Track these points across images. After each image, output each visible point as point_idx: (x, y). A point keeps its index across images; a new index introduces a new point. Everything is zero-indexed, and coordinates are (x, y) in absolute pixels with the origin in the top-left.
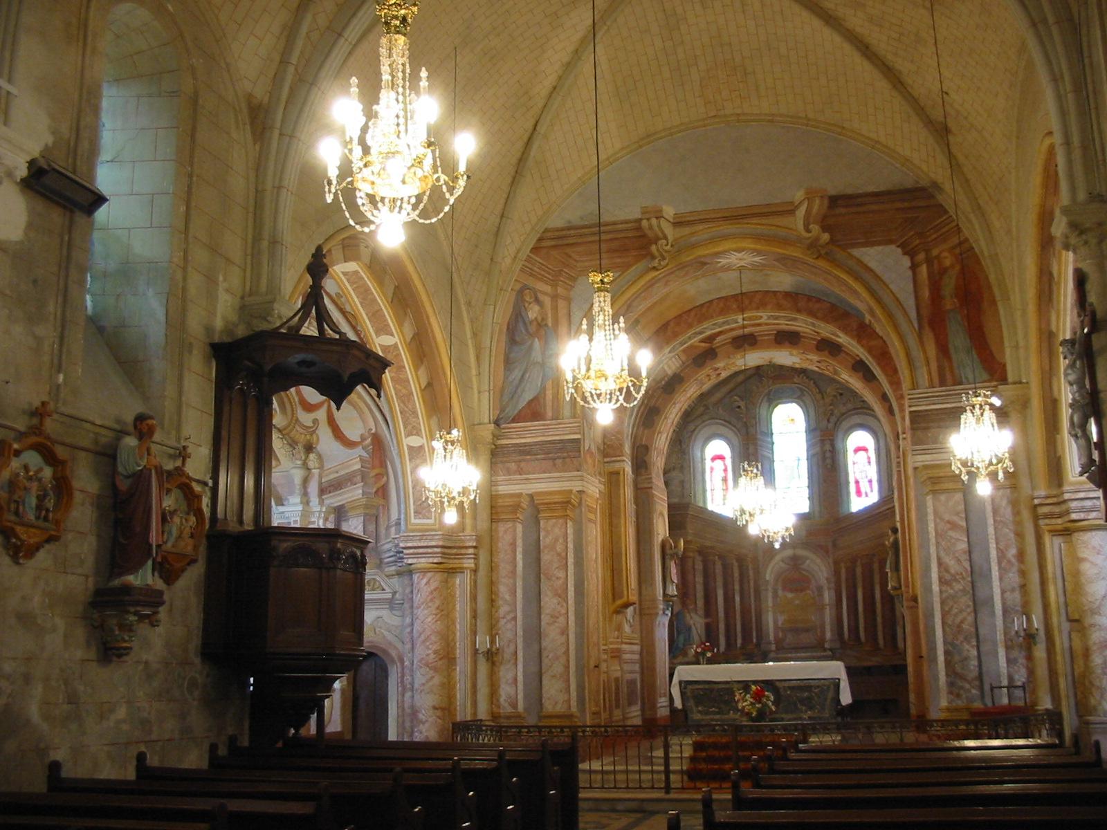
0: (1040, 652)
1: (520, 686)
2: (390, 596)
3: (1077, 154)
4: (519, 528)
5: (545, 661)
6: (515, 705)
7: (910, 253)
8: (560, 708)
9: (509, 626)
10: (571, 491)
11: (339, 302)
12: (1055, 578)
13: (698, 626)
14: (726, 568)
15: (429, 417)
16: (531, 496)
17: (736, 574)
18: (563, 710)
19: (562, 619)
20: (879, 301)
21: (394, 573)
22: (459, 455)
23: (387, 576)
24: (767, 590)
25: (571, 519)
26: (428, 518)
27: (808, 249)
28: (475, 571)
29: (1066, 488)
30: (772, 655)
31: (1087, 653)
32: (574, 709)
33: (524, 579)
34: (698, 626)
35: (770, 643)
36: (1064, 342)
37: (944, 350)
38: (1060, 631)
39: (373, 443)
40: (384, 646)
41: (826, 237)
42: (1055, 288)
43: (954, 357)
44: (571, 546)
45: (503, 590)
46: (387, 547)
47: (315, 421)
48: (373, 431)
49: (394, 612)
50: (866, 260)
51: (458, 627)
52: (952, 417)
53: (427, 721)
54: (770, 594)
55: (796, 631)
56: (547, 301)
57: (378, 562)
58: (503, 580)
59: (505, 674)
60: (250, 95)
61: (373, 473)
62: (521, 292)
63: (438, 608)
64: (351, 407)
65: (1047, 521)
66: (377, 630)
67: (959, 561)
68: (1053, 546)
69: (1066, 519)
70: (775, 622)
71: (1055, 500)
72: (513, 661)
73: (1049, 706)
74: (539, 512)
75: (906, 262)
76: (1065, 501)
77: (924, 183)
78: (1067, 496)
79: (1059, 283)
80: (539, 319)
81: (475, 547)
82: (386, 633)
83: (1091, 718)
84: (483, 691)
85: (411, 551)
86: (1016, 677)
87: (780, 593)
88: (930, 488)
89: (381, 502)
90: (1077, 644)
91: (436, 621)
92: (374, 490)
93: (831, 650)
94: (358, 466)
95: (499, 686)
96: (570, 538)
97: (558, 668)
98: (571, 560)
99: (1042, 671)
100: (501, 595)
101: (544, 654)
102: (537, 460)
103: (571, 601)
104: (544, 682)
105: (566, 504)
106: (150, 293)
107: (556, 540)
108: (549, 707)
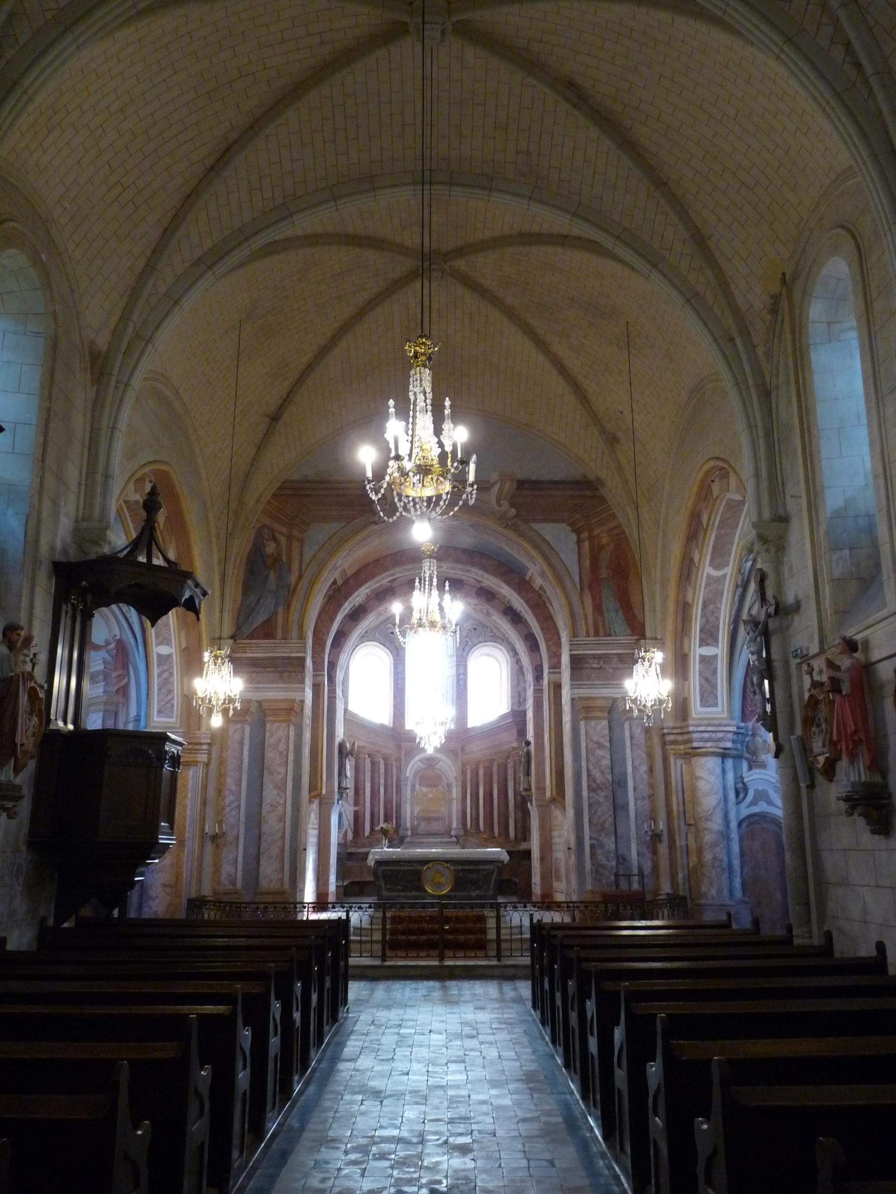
0: (663, 849)
1: (240, 867)
3: (764, 484)
4: (247, 729)
5: (264, 845)
6: (234, 884)
7: (577, 531)
8: (274, 886)
9: (233, 813)
12: (677, 788)
13: (348, 813)
14: (373, 764)
15: (179, 631)
16: (260, 703)
17: (382, 771)
19: (280, 808)
20: (551, 565)
22: (227, 668)
24: (406, 784)
25: (294, 724)
27: (499, 519)
28: (207, 765)
29: (690, 722)
30: (408, 839)
31: (700, 851)
32: (286, 886)
34: (348, 813)
35: (406, 829)
36: (745, 622)
37: (598, 608)
38: (680, 833)
39: (116, 648)
41: (513, 511)
42: (694, 570)
43: (606, 615)
44: (291, 746)
45: (230, 782)
48: (118, 637)
50: (543, 533)
51: (188, 813)
52: (628, 662)
53: (157, 897)
54: (409, 788)
55: (428, 820)
56: (283, 540)
58: (230, 773)
59: (227, 854)
60: (92, 343)
61: (114, 675)
62: (259, 532)
65: (673, 747)
67: (602, 773)
68: (676, 765)
69: (689, 745)
70: (412, 812)
71: (679, 731)
73: (669, 891)
74: (265, 716)
75: (574, 537)
76: (689, 733)
77: (592, 477)
78: (691, 729)
79: (698, 568)
80: (275, 554)
81: (209, 744)
83: (703, 901)
84: (208, 868)
86: (645, 867)
87: (417, 787)
88: (583, 715)
89: (121, 700)
90: (692, 843)
92: (116, 689)
93: (456, 836)
94: (101, 667)
96: (292, 740)
97: (275, 851)
98: (291, 757)
99: (664, 864)
101: (263, 838)
102: (268, 672)
103: (289, 794)
104: (262, 862)
106: (10, 512)
107: (280, 740)
108: (264, 884)
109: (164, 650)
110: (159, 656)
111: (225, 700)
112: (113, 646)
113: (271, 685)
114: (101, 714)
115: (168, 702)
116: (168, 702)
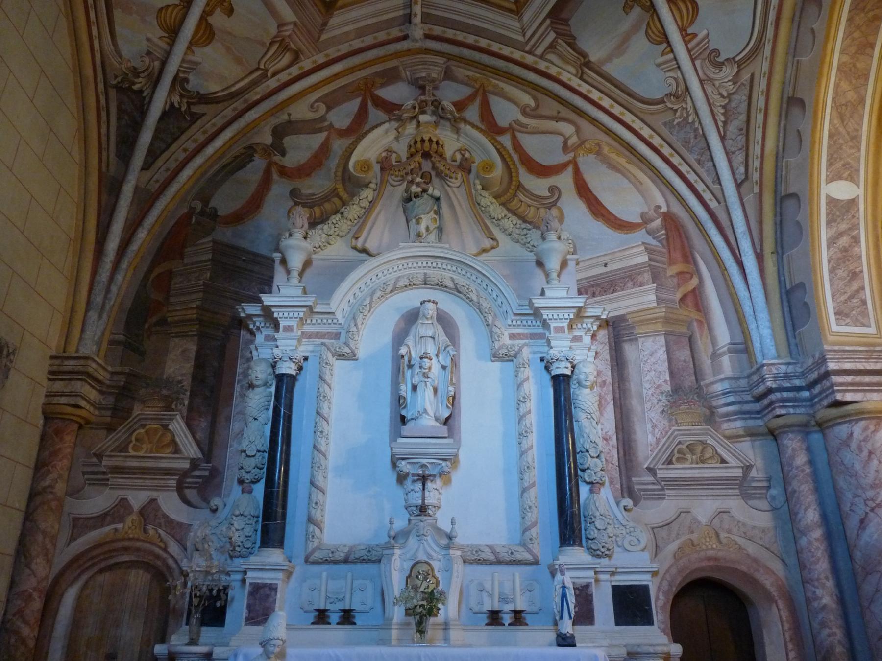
2: (739, 473)
11: (81, 355)
21: (741, 432)
23: (728, 438)
26: (864, 325)
40: (743, 568)
46: (719, 387)
47: (553, 189)
49: (750, 503)
57: (708, 412)
61: (672, 270)
64: (619, 175)
66: (723, 535)
82: (741, 541)
85: (849, 379)
89: (694, 315)
92: (678, 296)
109: (842, 190)
110: (832, 202)
112: (658, 223)
114: (662, 340)
115: (852, 297)
116: (852, 297)
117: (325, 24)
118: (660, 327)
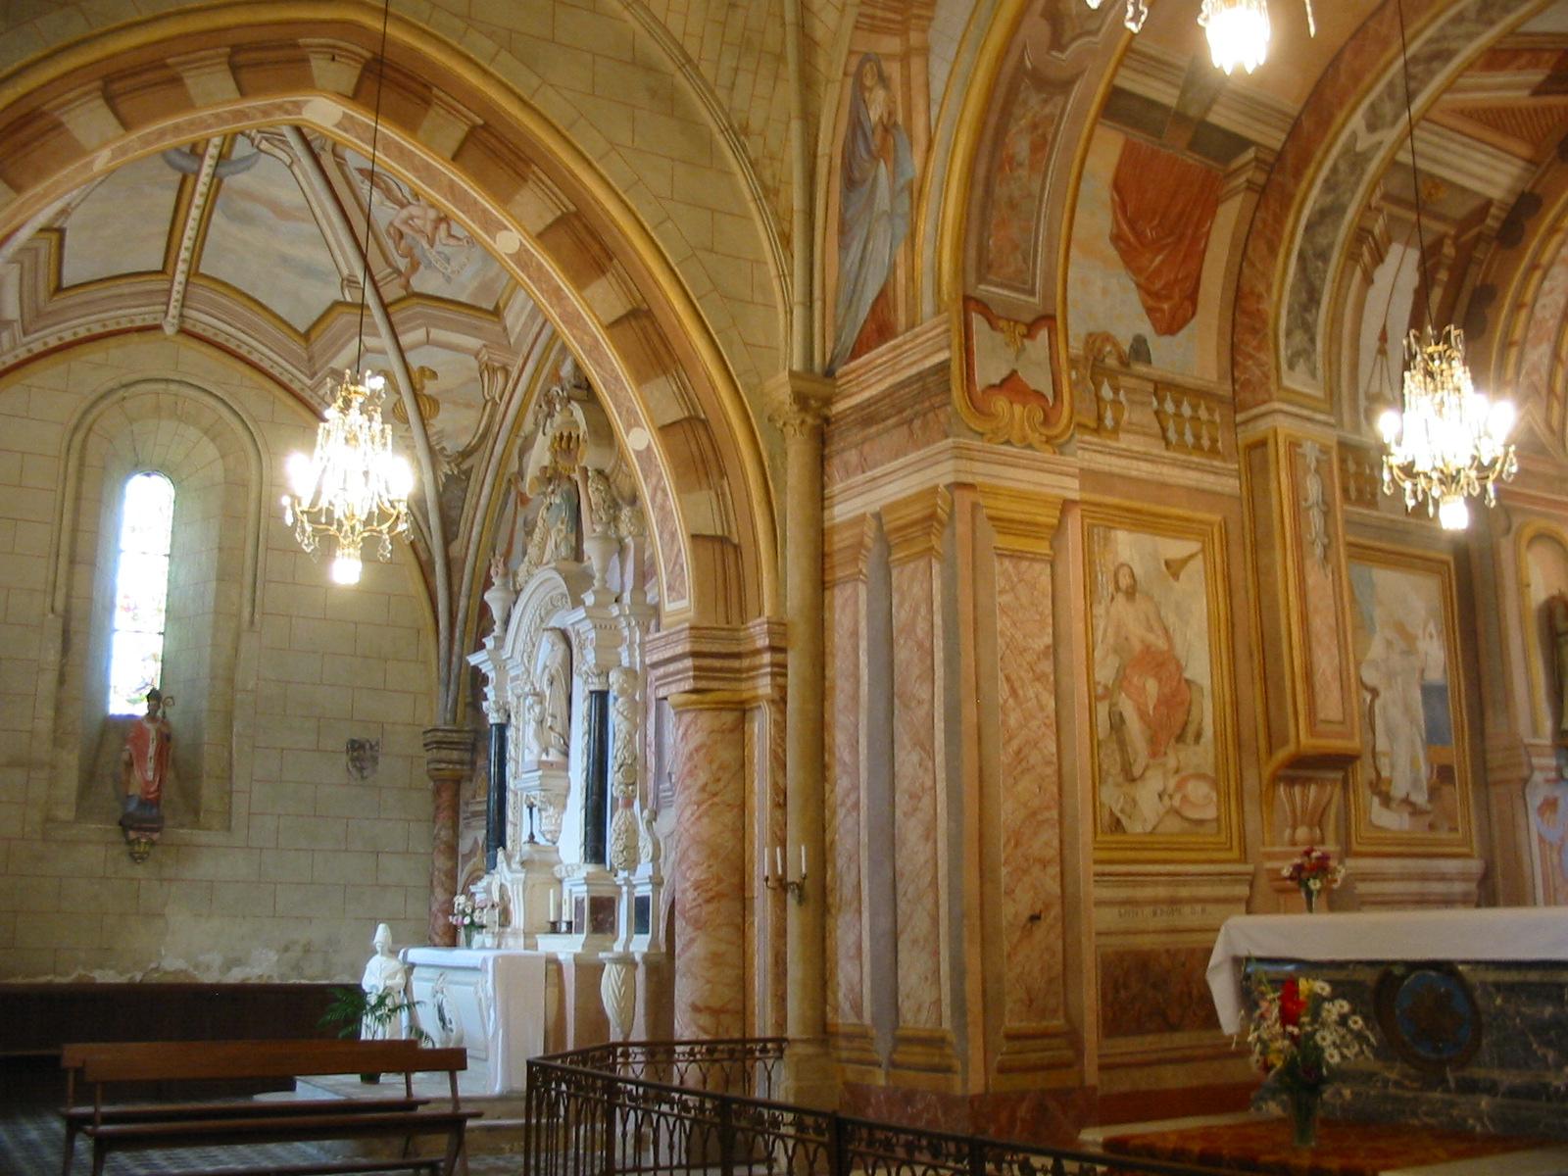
4: (862, 589)
6: (858, 1009)
10: (936, 487)
18: (928, 1026)
19: (926, 800)
33: (870, 711)
63: (703, 789)
72: (855, 904)
91: (699, 818)
95: (837, 963)
100: (838, 755)
102: (887, 431)
105: (930, 521)
107: (916, 611)
111: (371, 514)
113: (896, 464)
117: (505, 329)
118: (769, 670)
